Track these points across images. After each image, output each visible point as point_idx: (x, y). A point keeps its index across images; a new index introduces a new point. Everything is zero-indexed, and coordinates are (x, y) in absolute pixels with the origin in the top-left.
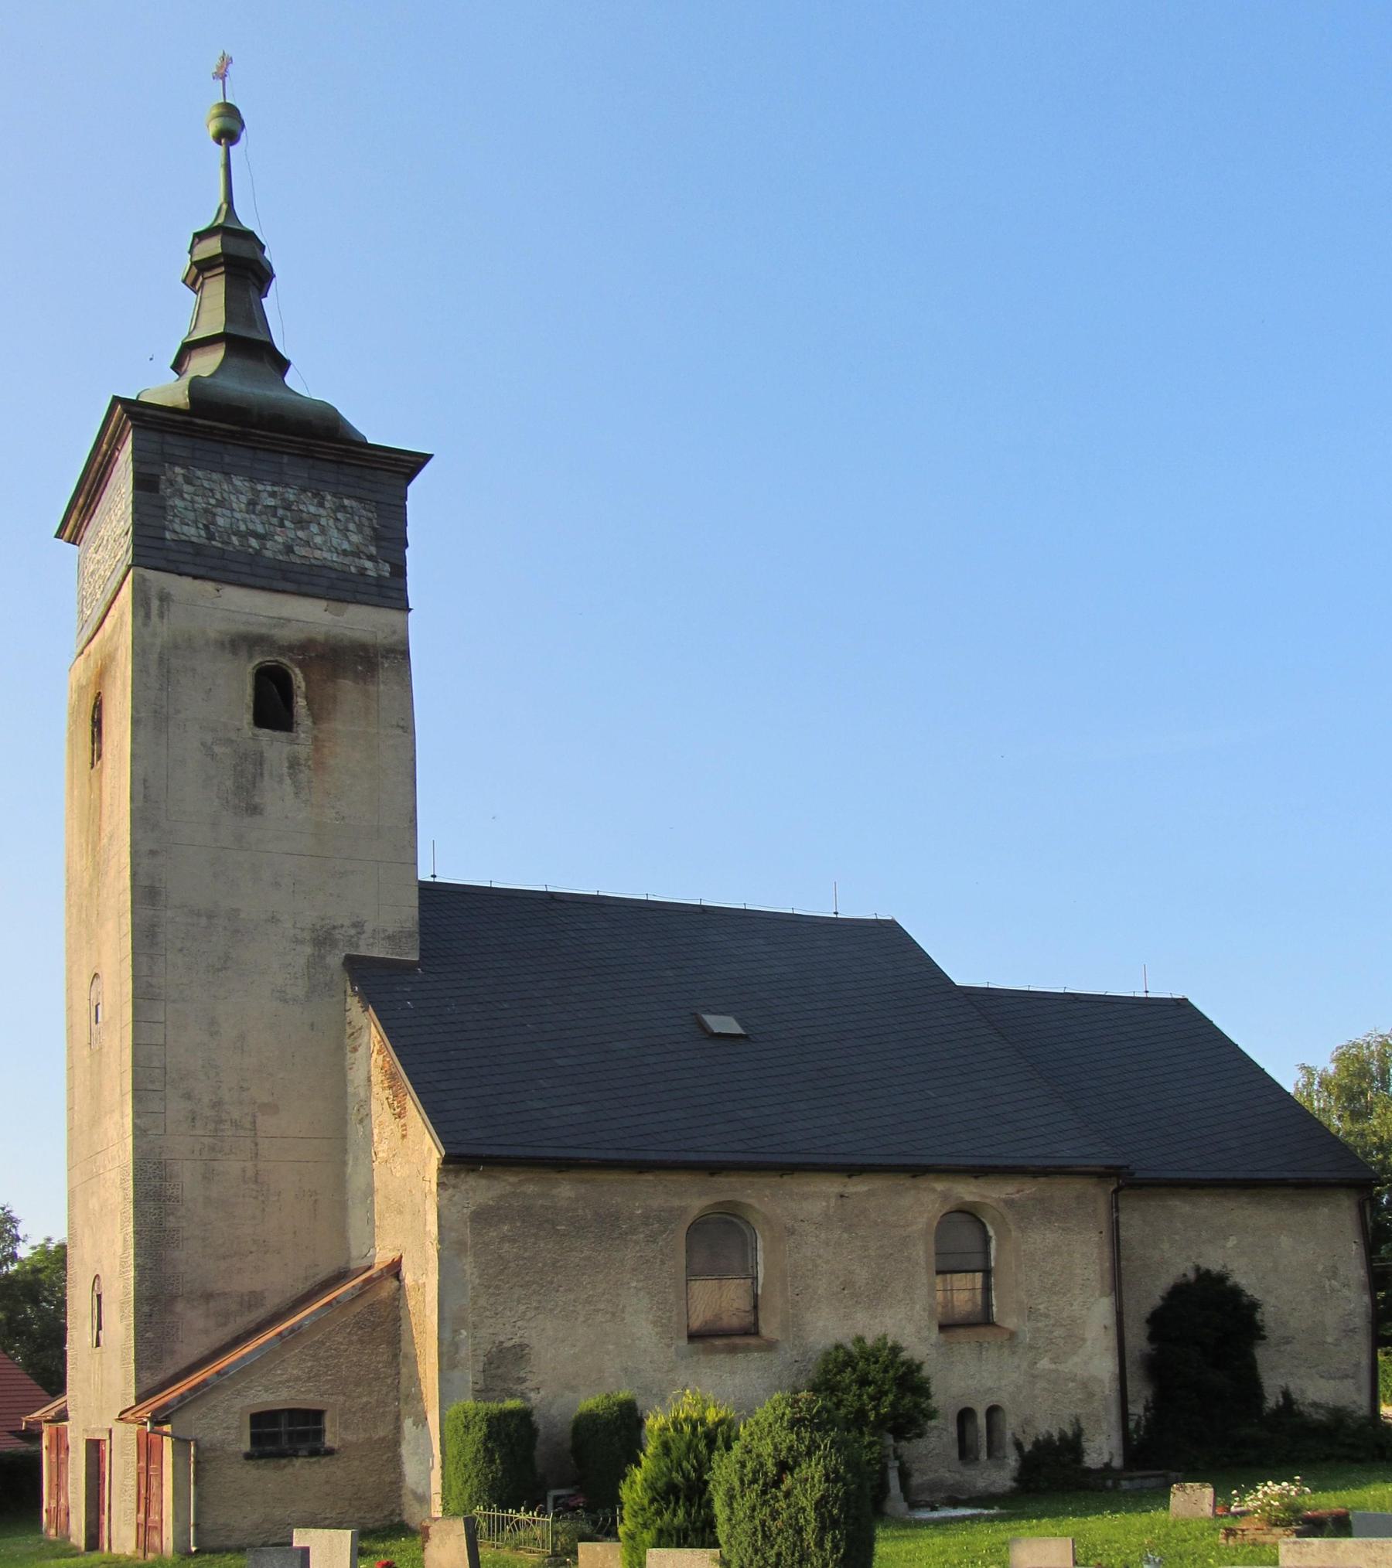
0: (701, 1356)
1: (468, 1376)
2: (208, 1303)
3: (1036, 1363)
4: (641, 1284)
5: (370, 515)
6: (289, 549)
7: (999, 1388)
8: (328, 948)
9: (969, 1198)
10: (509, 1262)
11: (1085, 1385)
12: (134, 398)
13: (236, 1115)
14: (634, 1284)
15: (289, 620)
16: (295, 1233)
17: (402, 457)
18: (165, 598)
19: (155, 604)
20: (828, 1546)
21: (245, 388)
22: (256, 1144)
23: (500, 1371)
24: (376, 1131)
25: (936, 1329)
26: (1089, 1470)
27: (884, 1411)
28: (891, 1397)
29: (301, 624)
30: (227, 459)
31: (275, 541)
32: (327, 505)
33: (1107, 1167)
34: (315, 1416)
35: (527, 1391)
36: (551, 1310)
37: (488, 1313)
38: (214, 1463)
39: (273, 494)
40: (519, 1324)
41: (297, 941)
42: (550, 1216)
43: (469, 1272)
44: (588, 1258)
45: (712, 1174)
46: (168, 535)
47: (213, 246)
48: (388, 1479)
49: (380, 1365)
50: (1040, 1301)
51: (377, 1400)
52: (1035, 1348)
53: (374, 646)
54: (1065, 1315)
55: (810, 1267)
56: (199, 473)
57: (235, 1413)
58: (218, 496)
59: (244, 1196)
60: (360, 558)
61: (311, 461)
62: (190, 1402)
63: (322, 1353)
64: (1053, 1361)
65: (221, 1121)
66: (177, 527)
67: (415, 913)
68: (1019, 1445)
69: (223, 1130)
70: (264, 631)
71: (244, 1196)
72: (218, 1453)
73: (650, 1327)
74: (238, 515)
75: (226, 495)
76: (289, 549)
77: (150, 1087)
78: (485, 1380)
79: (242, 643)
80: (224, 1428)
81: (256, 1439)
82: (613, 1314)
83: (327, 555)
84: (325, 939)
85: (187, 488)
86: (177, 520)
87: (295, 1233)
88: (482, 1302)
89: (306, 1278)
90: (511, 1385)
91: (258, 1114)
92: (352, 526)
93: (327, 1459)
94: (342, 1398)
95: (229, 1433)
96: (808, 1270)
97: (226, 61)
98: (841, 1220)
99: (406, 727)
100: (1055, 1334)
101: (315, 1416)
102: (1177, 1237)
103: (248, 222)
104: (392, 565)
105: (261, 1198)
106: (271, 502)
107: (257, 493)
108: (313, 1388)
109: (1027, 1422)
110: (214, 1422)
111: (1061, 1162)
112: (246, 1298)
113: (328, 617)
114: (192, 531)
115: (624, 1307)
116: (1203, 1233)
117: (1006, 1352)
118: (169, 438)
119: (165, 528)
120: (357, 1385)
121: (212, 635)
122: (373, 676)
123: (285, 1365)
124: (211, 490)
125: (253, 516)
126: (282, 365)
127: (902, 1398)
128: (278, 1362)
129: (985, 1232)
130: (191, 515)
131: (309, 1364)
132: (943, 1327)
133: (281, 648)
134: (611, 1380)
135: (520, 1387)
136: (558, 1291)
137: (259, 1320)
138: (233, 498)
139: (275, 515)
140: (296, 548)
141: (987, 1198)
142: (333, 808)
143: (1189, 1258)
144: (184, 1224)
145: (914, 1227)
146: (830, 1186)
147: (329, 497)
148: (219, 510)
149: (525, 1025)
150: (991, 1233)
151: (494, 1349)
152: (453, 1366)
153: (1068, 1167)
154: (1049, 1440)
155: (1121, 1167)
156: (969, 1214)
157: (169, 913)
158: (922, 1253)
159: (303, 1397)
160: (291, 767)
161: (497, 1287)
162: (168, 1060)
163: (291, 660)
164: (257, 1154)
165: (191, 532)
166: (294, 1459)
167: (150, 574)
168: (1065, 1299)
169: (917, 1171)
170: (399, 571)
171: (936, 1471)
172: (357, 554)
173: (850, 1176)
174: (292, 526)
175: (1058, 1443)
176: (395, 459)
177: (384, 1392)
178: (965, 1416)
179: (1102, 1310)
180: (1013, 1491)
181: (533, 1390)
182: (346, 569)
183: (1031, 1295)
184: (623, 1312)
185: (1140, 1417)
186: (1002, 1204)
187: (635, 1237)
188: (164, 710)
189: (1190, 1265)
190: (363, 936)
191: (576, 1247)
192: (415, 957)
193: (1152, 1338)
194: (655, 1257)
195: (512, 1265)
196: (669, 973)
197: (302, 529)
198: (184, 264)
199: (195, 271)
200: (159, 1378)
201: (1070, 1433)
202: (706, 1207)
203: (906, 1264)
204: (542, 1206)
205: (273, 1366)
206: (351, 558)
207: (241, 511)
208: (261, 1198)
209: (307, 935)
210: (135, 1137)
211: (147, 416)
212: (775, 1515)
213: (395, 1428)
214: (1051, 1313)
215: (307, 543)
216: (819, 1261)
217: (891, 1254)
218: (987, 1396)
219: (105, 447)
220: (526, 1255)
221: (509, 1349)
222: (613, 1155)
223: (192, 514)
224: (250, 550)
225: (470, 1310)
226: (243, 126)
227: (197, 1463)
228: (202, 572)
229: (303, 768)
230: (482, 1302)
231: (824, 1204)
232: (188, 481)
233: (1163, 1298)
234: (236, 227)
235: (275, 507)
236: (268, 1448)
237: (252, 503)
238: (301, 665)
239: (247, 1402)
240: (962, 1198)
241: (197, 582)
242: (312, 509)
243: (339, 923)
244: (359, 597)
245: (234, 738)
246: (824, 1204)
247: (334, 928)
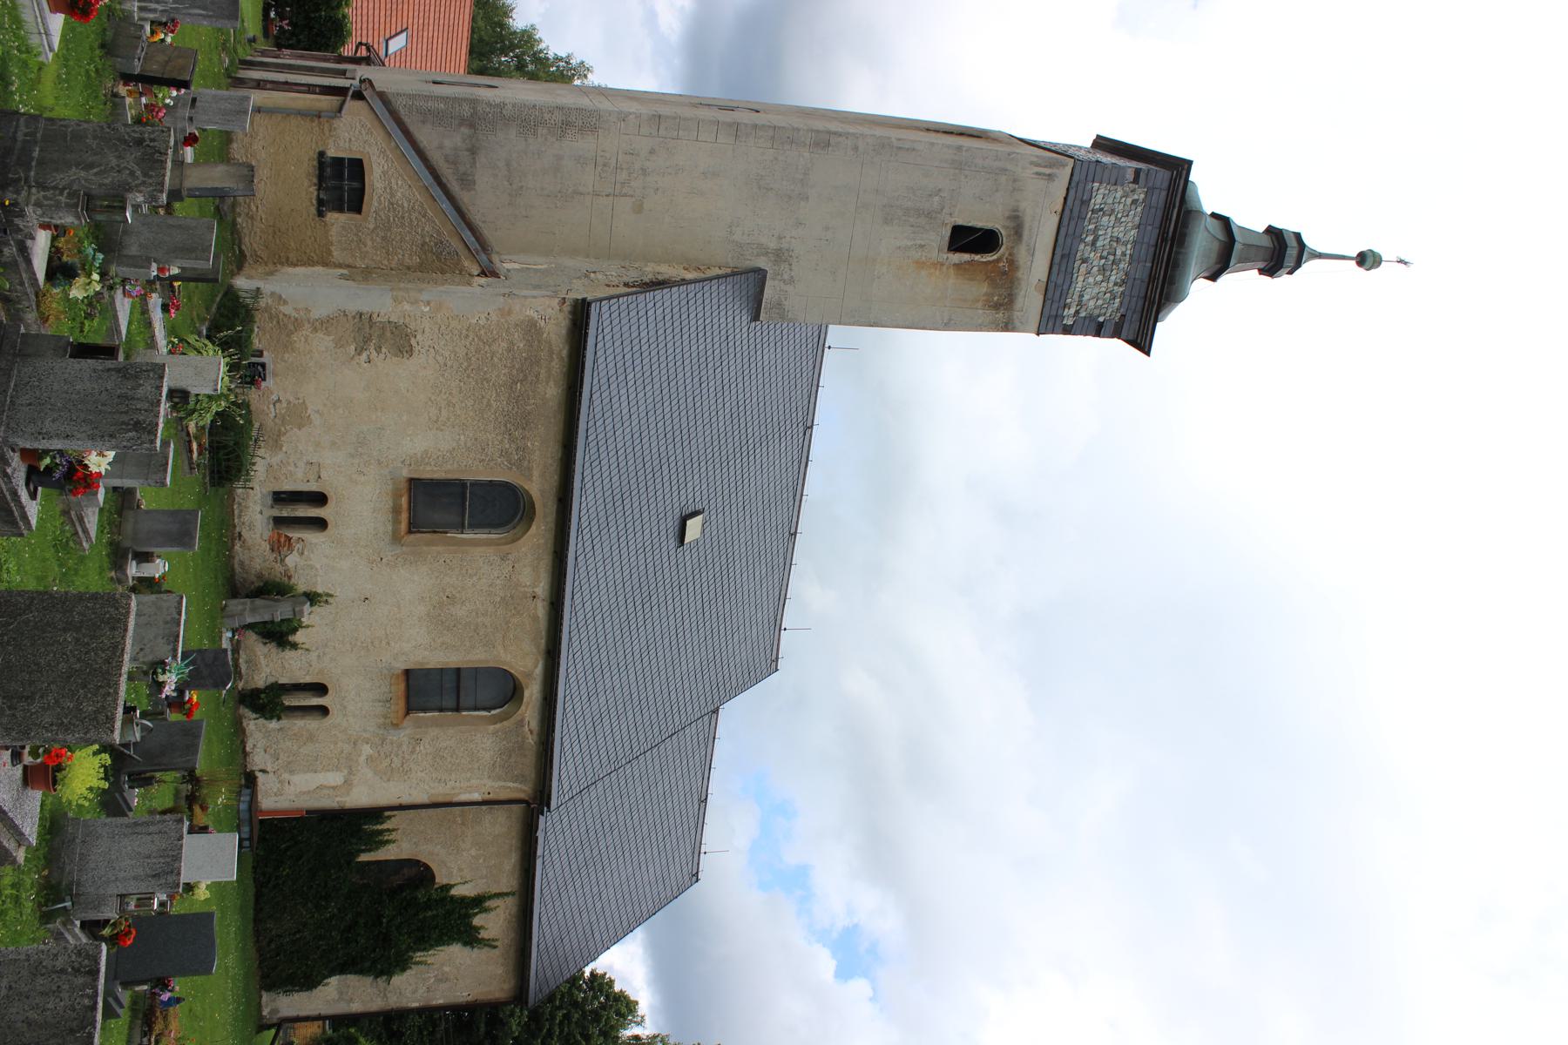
0: (391, 487)
5: (1108, 315)
6: (1084, 261)
8: (773, 259)
9: (527, 694)
16: (527, 217)
18: (1050, 177)
19: (1048, 171)
21: (1201, 243)
22: (607, 196)
23: (388, 334)
29: (1029, 263)
32: (1116, 288)
38: (317, 129)
39: (1124, 254)
40: (432, 350)
44: (489, 405)
46: (1096, 185)
48: (291, 255)
49: (400, 257)
52: (383, 743)
55: (470, 571)
56: (1139, 209)
57: (364, 148)
58: (1123, 219)
61: (1147, 280)
66: (1101, 191)
71: (561, 183)
78: (381, 322)
80: (350, 139)
81: (338, 161)
83: (1080, 285)
85: (1129, 201)
86: (1107, 192)
87: (527, 217)
90: (374, 341)
91: (634, 199)
92: (1100, 302)
94: (371, 226)
95: (345, 142)
98: (512, 597)
100: (395, 758)
102: (481, 861)
103: (1309, 267)
105: (559, 195)
106: (1119, 252)
108: (383, 205)
112: (470, 178)
114: (1099, 199)
115: (442, 430)
117: (381, 721)
118: (1164, 193)
119: (1101, 183)
120: (384, 238)
121: (1023, 205)
124: (1127, 216)
125: (1109, 240)
128: (409, 182)
129: (495, 708)
131: (406, 205)
134: (374, 417)
136: (460, 381)
138: (1122, 229)
139: (1108, 254)
140: (1085, 265)
141: (527, 707)
144: (539, 140)
147: (1121, 289)
148: (1113, 218)
150: (493, 712)
157: (807, 155)
159: (375, 198)
161: (467, 336)
162: (685, 142)
164: (599, 195)
165: (1097, 200)
168: (428, 766)
170: (1067, 330)
172: (1080, 303)
174: (1101, 264)
176: (1147, 334)
182: (1070, 295)
186: (519, 719)
188: (966, 168)
194: (487, 455)
205: (406, 178)
209: (785, 246)
213: (340, 264)
218: (338, 706)
223: (1111, 202)
224: (1084, 236)
226: (1368, 270)
228: (1076, 178)
231: (528, 584)
232: (1134, 202)
234: (1304, 259)
235: (1115, 255)
237: (1118, 240)
239: (374, 158)
240: (527, 688)
241: (1061, 200)
243: (793, 267)
244: (1049, 302)
247: (791, 265)
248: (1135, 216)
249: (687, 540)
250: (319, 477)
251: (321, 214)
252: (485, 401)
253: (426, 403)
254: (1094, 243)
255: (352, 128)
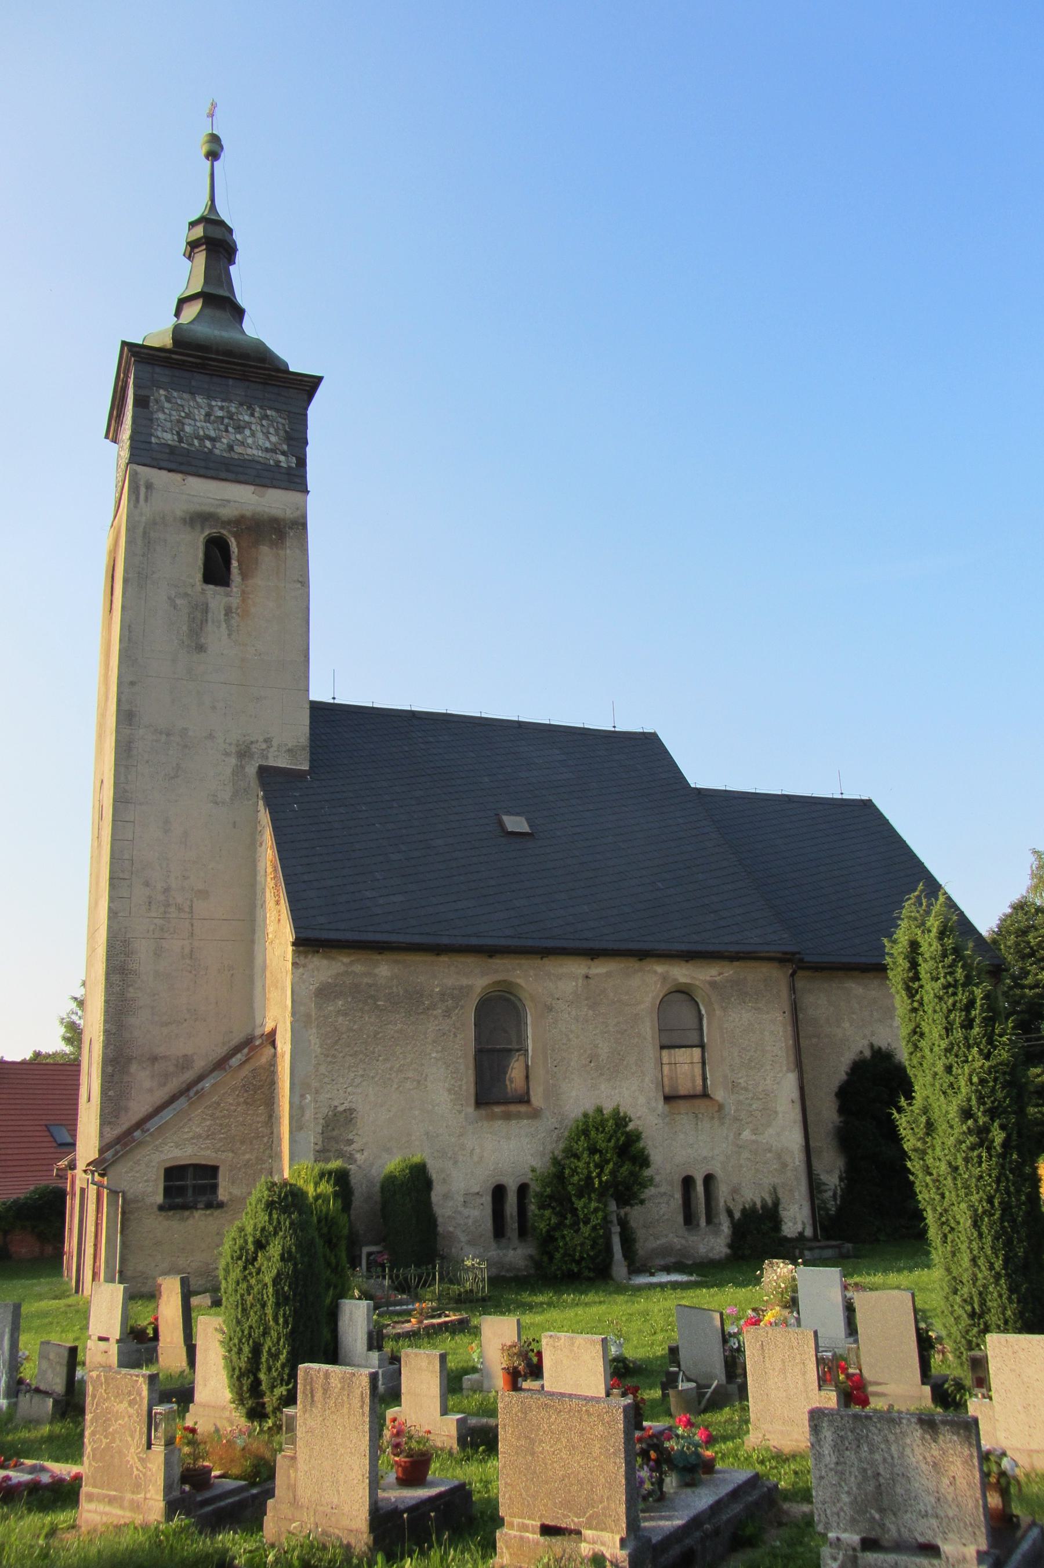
1: (311, 1137)
2: (153, 1065)
3: (740, 1134)
4: (439, 1055)
5: (283, 421)
6: (231, 448)
7: (712, 1158)
9: (683, 980)
10: (342, 1033)
11: (779, 1156)
12: (141, 343)
13: (179, 900)
14: (434, 1055)
15: (229, 501)
17: (306, 379)
18: (149, 486)
19: (143, 490)
20: (281, 1321)
21: (213, 332)
22: (192, 925)
23: (335, 1133)
24: (268, 915)
25: (661, 1101)
26: (785, 1238)
27: (604, 1179)
28: (611, 1165)
30: (194, 383)
31: (222, 443)
32: (257, 414)
33: (785, 953)
34: (211, 1171)
35: (353, 1152)
36: (373, 1077)
37: (326, 1080)
39: (221, 408)
40: (349, 1090)
41: (227, 754)
42: (373, 993)
43: (313, 1042)
44: (400, 1031)
45: (491, 956)
46: (153, 440)
47: (199, 232)
50: (740, 1075)
51: (257, 1158)
53: (284, 520)
54: (760, 1089)
55: (565, 1042)
56: (175, 394)
57: (153, 1167)
59: (182, 970)
60: (277, 453)
62: (122, 1155)
63: (218, 1114)
64: (755, 1132)
65: (169, 905)
66: (159, 434)
67: (306, 730)
68: (730, 1213)
69: (169, 913)
70: (212, 510)
72: (140, 1204)
73: (446, 1094)
74: (198, 424)
75: (191, 409)
76: (231, 448)
77: (121, 876)
79: (199, 519)
81: (168, 1191)
82: (419, 1082)
83: (255, 452)
84: (245, 752)
85: (167, 405)
86: (160, 429)
88: (323, 1069)
89: (224, 1044)
91: (195, 899)
92: (272, 430)
93: (219, 1211)
94: (231, 1155)
96: (563, 1044)
97: (214, 106)
99: (304, 582)
101: (211, 1171)
102: (854, 1016)
103: (224, 214)
104: (298, 458)
105: (194, 972)
106: (220, 413)
107: (211, 407)
109: (735, 1190)
110: (138, 1175)
111: (749, 948)
112: (181, 1061)
113: (254, 498)
116: (875, 1013)
117: (716, 1123)
118: (158, 370)
119: (152, 435)
120: (242, 1142)
121: (179, 513)
122: (282, 543)
123: (191, 1123)
124: (182, 406)
125: (208, 424)
126: (239, 313)
127: (621, 1167)
129: (699, 1011)
130: (169, 425)
131: (208, 1123)
132: (668, 1099)
133: (223, 522)
135: (348, 1149)
137: (189, 1081)
138: (196, 411)
139: (222, 423)
142: (254, 646)
143: (865, 1037)
145: (642, 1006)
146: (577, 968)
147: (258, 409)
148: (187, 421)
149: (374, 824)
150: (703, 1012)
151: (330, 1113)
152: (300, 1128)
153: (754, 952)
154: (754, 1208)
155: (794, 954)
156: (684, 992)
157: (141, 732)
158: (648, 1029)
160: (226, 615)
161: (334, 1056)
162: (135, 853)
163: (230, 531)
165: (169, 438)
166: (195, 1212)
167: (141, 469)
168: (759, 1074)
169: (642, 955)
170: (302, 462)
171: (667, 1236)
172: (274, 451)
173: (592, 959)
175: (760, 1212)
177: (261, 1150)
178: (688, 1182)
179: (789, 1084)
180: (728, 1258)
181: (358, 1151)
183: (733, 1070)
184: (426, 1080)
185: (836, 1187)
187: (435, 1012)
189: (866, 1042)
190: (271, 750)
191: (391, 1021)
192: (305, 767)
193: (841, 1110)
194: (450, 1031)
195: (344, 1036)
196: (486, 779)
197: (240, 433)
198: (183, 246)
199: (189, 248)
200: (116, 1132)
201: (769, 1202)
202: (487, 986)
203: (636, 1040)
204: (367, 984)
206: (271, 454)
207: (201, 421)
208: (194, 972)
209: (233, 749)
210: (109, 918)
211: (143, 353)
212: (250, 1288)
214: (750, 1087)
215: (242, 444)
216: (571, 1036)
217: (626, 1030)
219: (122, 375)
220: (355, 1027)
221: (341, 1113)
222: (417, 939)
225: (313, 1077)
227: (123, 1213)
228: (173, 466)
229: (234, 615)
230: (323, 1069)
231: (574, 984)
232: (168, 400)
233: (847, 1073)
235: (222, 418)
236: (178, 1200)
237: (208, 415)
238: (236, 536)
240: (676, 980)
241: (171, 474)
242: (247, 418)
245: (189, 592)
246: (574, 984)
247: (252, 743)
248: (182, 398)
249: (526, 828)
250: (478, 1193)
251: (221, 1205)
252: (396, 1035)
253: (401, 1092)
254: (213, 440)
255: (134, 1180)
